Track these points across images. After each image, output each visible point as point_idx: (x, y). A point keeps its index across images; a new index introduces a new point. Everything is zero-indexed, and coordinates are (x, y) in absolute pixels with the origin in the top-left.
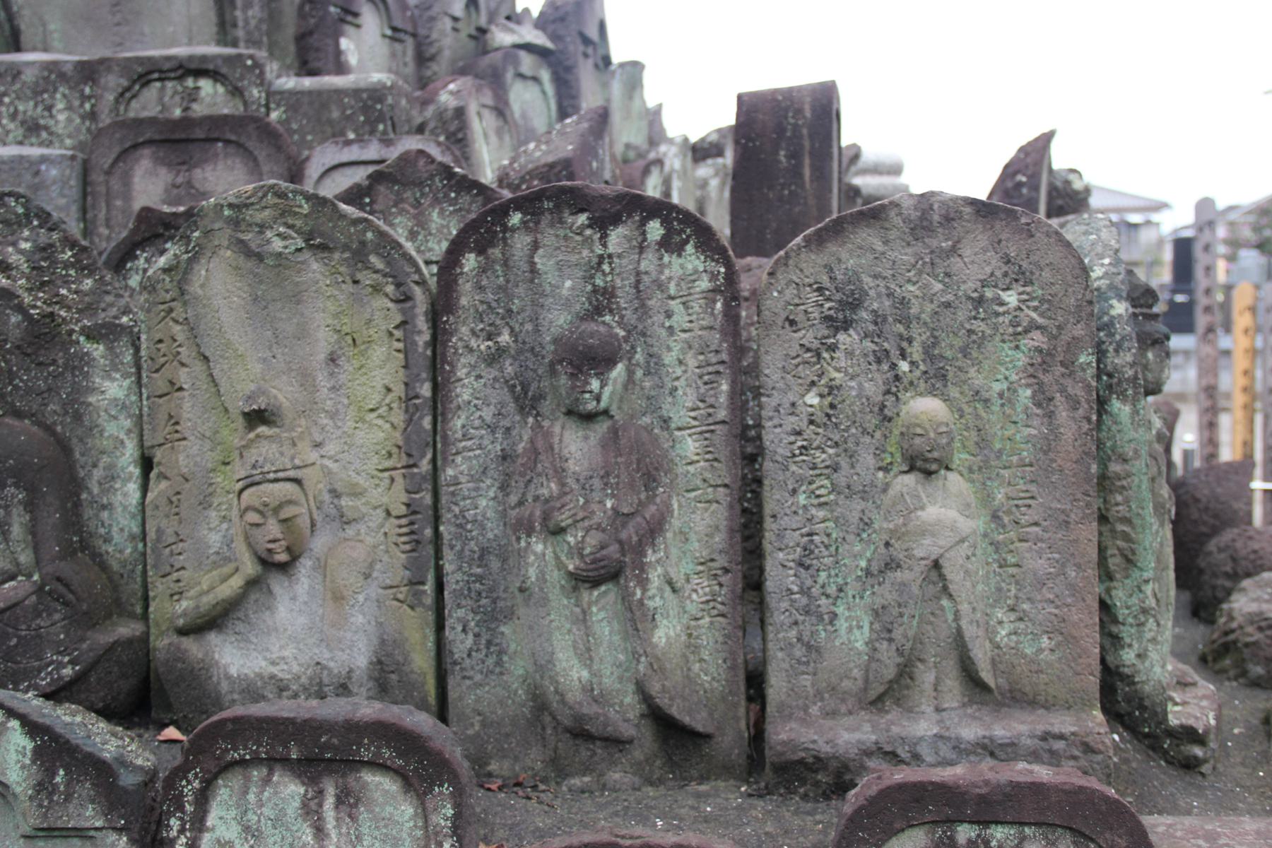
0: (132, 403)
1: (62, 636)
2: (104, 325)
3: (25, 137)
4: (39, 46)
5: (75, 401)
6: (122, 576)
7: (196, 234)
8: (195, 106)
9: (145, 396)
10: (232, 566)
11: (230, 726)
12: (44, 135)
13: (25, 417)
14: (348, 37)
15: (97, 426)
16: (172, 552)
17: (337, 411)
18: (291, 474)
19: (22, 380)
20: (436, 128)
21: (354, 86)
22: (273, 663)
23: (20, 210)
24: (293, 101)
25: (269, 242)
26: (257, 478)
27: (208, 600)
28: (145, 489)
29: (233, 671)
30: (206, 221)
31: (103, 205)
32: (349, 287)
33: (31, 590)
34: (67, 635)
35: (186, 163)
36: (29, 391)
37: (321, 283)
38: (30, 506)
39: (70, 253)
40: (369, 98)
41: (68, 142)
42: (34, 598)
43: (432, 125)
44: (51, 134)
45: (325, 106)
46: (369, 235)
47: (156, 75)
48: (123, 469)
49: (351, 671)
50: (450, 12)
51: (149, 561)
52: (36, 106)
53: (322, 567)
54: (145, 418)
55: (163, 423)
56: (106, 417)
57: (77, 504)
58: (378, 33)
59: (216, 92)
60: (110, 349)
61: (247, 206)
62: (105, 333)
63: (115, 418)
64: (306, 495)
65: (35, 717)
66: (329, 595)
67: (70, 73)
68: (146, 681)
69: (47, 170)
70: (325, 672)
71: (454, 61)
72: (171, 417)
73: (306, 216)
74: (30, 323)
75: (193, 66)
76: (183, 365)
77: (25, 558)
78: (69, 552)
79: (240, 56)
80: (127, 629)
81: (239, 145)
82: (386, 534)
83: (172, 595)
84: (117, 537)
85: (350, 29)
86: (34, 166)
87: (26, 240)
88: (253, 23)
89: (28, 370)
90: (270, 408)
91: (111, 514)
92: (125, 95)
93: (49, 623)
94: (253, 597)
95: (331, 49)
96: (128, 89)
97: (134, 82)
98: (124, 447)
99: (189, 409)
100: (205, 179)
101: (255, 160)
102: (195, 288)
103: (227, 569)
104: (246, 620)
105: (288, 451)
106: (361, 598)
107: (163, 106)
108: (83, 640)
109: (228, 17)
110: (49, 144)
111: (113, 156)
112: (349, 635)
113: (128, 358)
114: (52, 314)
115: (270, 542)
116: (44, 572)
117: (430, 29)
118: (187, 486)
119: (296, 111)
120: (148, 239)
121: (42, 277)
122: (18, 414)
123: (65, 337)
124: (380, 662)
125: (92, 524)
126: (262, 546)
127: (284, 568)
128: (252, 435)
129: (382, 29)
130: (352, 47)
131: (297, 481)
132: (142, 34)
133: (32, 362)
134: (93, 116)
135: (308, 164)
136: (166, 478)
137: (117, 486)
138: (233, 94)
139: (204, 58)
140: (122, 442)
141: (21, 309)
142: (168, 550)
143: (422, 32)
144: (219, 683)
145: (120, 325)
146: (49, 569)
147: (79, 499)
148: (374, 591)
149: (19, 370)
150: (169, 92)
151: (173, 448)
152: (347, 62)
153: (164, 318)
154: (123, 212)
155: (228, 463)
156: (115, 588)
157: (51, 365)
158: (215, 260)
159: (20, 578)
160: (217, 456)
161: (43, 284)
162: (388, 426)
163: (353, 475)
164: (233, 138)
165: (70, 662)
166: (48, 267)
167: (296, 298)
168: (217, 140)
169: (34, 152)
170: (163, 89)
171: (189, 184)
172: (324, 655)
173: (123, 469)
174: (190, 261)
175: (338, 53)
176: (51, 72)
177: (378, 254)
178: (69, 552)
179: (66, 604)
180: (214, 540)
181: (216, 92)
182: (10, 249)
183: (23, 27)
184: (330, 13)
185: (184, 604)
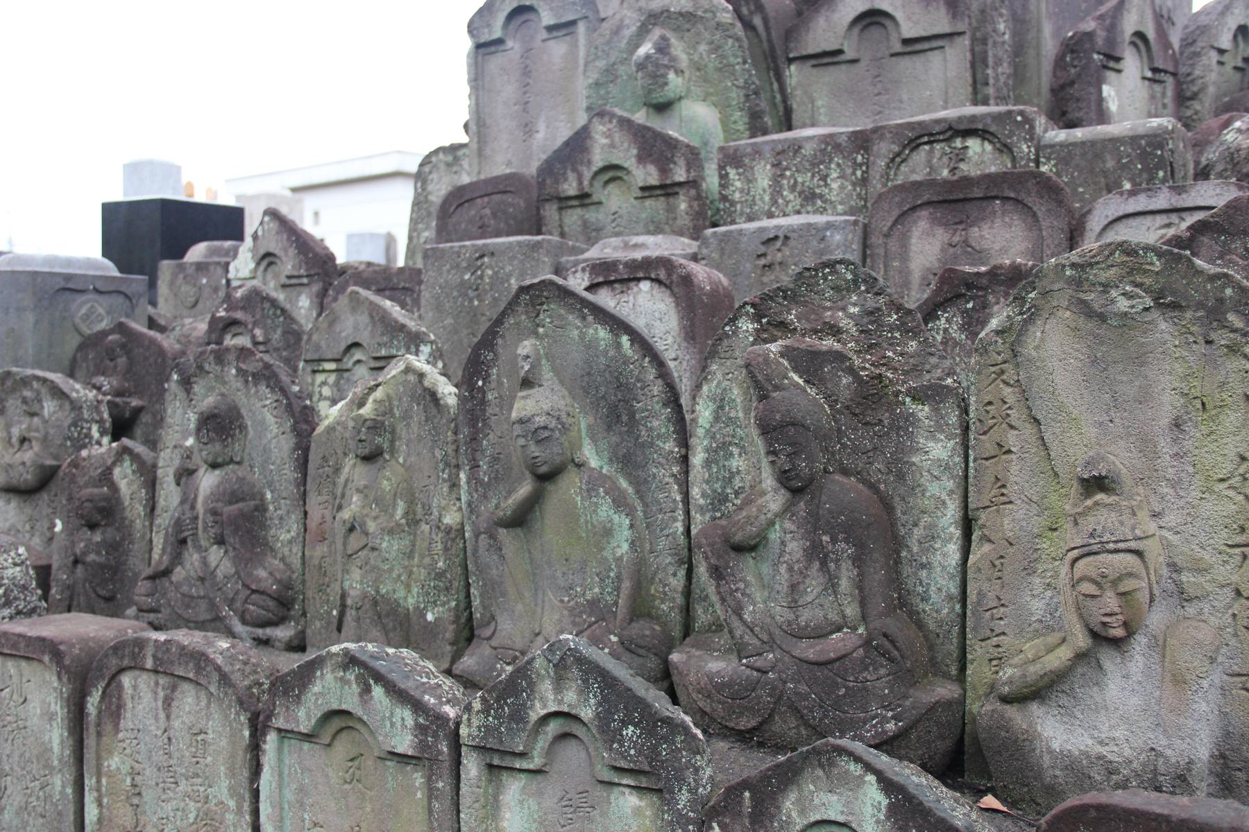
0: (955, 464)
1: (886, 691)
2: (930, 387)
3: (802, 206)
4: (808, 121)
5: (898, 460)
6: (938, 636)
7: (1032, 295)
8: (962, 166)
9: (971, 458)
10: (1057, 636)
11: (1093, 813)
12: (819, 202)
13: (851, 475)
14: (1110, 84)
15: (919, 486)
16: (992, 615)
17: (1180, 479)
18: (1133, 545)
19: (849, 439)
20: (1226, 170)
21: (1130, 134)
22: (1101, 743)
23: (849, 277)
24: (1064, 153)
25: (1113, 301)
26: (1095, 548)
27: (1035, 670)
28: (966, 551)
29: (1056, 745)
30: (1045, 282)
31: (881, 266)
32: (1201, 348)
33: (860, 642)
34: (891, 692)
35: (965, 223)
36: (855, 449)
37: (1169, 345)
38: (858, 561)
39: (895, 317)
40: (1148, 144)
41: (840, 208)
42: (861, 651)
43: (1219, 167)
44: (825, 201)
45: (1098, 156)
46: (1229, 291)
47: (926, 139)
48: (943, 529)
49: (1191, 762)
50: (1216, 45)
51: (968, 623)
52: (813, 176)
53: (1160, 646)
54: (971, 480)
55: (989, 485)
56: (929, 478)
57: (898, 562)
58: (1138, 76)
59: (984, 150)
60: (936, 410)
61: (1091, 265)
62: (932, 394)
63: (937, 478)
64: (1147, 568)
65: (889, 774)
66: (1168, 677)
67: (844, 144)
68: (961, 741)
69: (832, 236)
70: (1161, 760)
71: (1218, 98)
72: (997, 479)
73: (1157, 273)
74: (859, 384)
75: (962, 127)
76: (1012, 427)
77: (852, 610)
78: (890, 610)
79: (1010, 112)
80: (945, 691)
81: (1017, 201)
82: (1234, 615)
83: (990, 660)
84: (934, 597)
85: (1111, 75)
86: (819, 232)
87: (855, 305)
88: (1002, 79)
89: (855, 429)
90: (1110, 475)
91: (929, 574)
92: (895, 161)
93: (875, 677)
94: (1080, 670)
95: (1093, 98)
96: (898, 155)
97: (904, 147)
98: (946, 508)
99: (1017, 473)
100: (982, 237)
101: (1034, 215)
102: (1029, 349)
103: (1053, 638)
104: (1071, 694)
105: (1129, 521)
106: (1205, 684)
107: (931, 168)
108: (905, 697)
109: (979, 76)
110: (823, 211)
111: (893, 219)
112: (1190, 723)
113: (953, 419)
114: (880, 374)
115: (1106, 615)
116: (871, 626)
117: (1192, 65)
118: (1011, 550)
119: (1067, 164)
120: (948, 300)
121: (870, 341)
122: (845, 472)
123: (892, 398)
124: (1223, 756)
125: (910, 582)
126: (1096, 619)
127: (1117, 643)
128: (1089, 502)
129: (1142, 70)
130: (1113, 93)
131: (1139, 553)
132: (901, 101)
133: (859, 422)
134: (864, 181)
135: (1090, 217)
136: (990, 541)
137: (937, 546)
138: (1001, 151)
139: (973, 118)
140: (944, 503)
141: (851, 371)
142: (989, 613)
143: (1183, 70)
144: (1041, 757)
145: (947, 387)
146: (876, 624)
147: (899, 557)
148: (1217, 677)
149: (846, 428)
150: (937, 154)
151: (998, 511)
152: (1108, 108)
153: (996, 379)
154: (900, 272)
155: (1056, 529)
156: (931, 647)
157: (876, 425)
158: (1053, 321)
159: (845, 630)
160: (1043, 521)
161: (871, 346)
162: (1241, 497)
163: (1197, 549)
164: (1012, 195)
165: (893, 717)
166: (876, 331)
167: (1140, 360)
168: (996, 197)
169: (820, 219)
170: (932, 151)
171: (966, 243)
172: (1161, 742)
173: (943, 529)
174: (1026, 322)
175: (1100, 100)
176: (827, 144)
177: (1237, 312)
178: (890, 610)
179: (892, 660)
180: (1037, 607)
181: (984, 150)
182: (840, 314)
183: (795, 106)
184: (1094, 60)
185: (1009, 671)
